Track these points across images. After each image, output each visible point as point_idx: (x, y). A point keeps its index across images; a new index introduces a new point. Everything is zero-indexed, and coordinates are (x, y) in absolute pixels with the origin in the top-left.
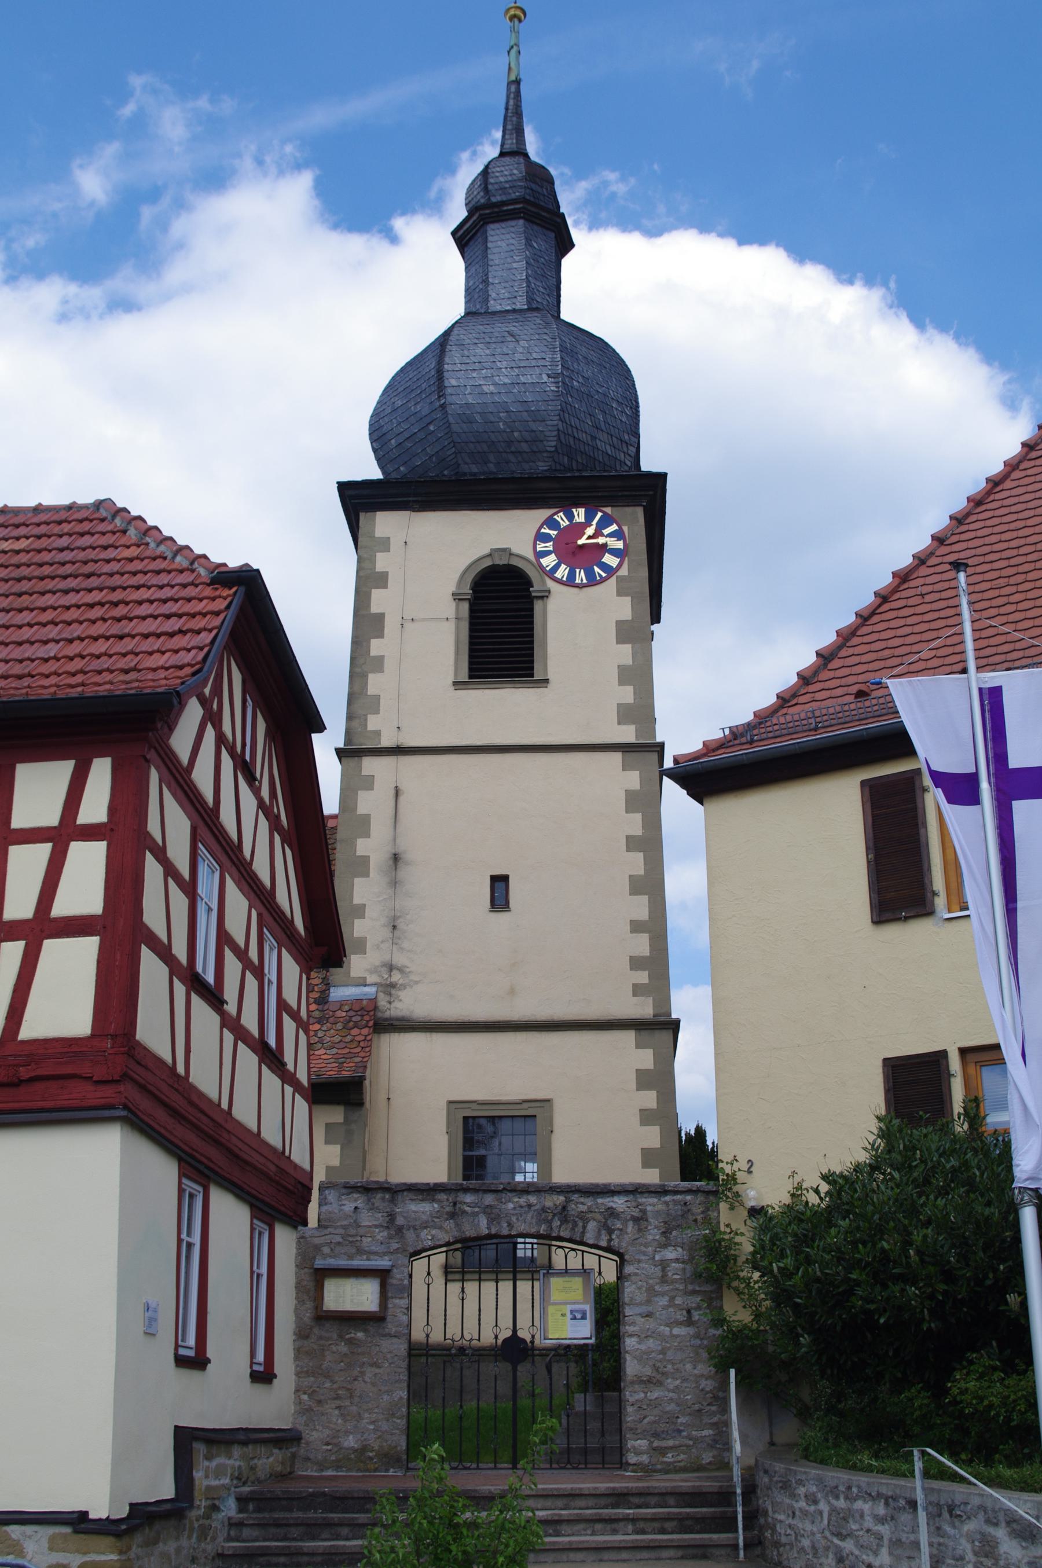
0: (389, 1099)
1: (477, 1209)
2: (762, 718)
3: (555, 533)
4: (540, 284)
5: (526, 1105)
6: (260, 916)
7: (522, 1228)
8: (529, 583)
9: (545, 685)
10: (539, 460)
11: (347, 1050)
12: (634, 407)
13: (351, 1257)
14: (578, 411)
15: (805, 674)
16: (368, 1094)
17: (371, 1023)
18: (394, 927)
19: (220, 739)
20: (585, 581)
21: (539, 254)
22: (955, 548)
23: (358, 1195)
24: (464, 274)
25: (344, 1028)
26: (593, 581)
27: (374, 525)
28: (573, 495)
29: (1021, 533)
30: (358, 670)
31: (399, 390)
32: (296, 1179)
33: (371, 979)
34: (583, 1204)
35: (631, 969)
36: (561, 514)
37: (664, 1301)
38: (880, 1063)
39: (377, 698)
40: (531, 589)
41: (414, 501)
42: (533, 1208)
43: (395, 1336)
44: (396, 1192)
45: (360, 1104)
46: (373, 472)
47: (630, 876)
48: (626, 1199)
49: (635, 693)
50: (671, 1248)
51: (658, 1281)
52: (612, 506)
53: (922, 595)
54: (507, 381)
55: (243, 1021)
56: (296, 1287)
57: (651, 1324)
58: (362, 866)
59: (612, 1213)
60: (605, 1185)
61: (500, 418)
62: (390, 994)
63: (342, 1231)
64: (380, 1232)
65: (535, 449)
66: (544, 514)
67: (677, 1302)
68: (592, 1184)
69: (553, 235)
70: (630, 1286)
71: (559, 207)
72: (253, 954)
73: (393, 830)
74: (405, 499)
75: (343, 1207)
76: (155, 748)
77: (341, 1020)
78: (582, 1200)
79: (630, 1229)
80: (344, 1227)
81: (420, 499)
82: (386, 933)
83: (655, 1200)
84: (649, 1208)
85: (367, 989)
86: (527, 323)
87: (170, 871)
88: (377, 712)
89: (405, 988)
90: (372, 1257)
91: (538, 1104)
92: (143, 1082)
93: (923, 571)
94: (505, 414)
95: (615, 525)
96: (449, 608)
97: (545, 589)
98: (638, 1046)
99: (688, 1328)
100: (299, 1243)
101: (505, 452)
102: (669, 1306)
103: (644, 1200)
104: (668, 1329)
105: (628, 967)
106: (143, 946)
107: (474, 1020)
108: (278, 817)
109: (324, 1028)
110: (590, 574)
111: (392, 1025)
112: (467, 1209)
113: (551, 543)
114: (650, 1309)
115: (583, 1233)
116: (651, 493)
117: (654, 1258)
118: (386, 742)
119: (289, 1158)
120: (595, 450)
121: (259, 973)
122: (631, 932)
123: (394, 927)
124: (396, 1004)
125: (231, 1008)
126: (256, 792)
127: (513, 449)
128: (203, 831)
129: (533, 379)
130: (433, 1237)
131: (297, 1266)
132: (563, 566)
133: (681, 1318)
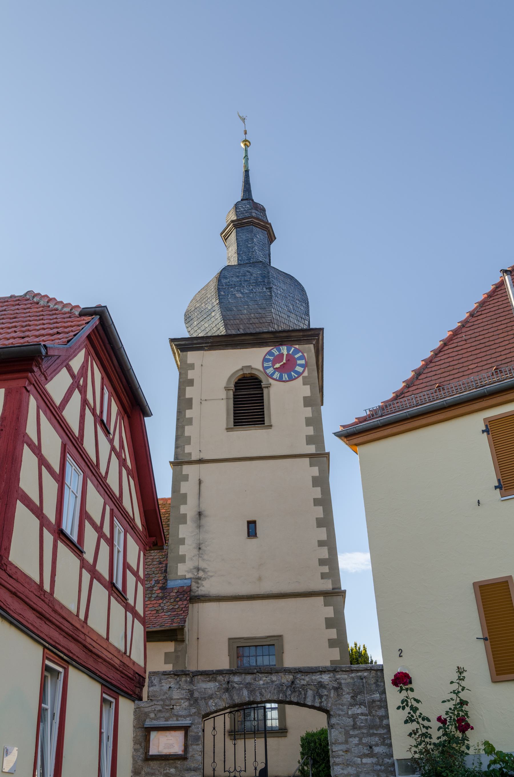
0: (198, 638)
1: (241, 686)
3: (272, 358)
4: (261, 253)
5: (269, 639)
6: (112, 510)
7: (268, 697)
8: (261, 382)
9: (270, 428)
10: (264, 327)
11: (176, 613)
12: (306, 303)
13: (167, 720)
14: (281, 304)
16: (187, 636)
17: (188, 598)
18: (200, 548)
19: (85, 402)
20: (287, 379)
21: (260, 240)
22: (479, 318)
23: (172, 680)
25: (174, 601)
26: (291, 379)
32: (134, 671)
33: (188, 576)
34: (304, 680)
36: (275, 349)
37: (356, 741)
39: (189, 438)
40: (262, 384)
41: (205, 346)
43: (193, 770)
45: (183, 641)
47: (317, 518)
48: (329, 676)
49: (314, 430)
50: (357, 706)
51: (351, 728)
53: (466, 340)
54: (247, 291)
55: (98, 568)
56: (133, 740)
57: (348, 756)
58: (183, 519)
59: (321, 685)
60: (316, 668)
62: (198, 583)
64: (184, 702)
65: (261, 321)
66: (267, 349)
67: (364, 742)
68: (308, 667)
70: (335, 731)
72: (106, 530)
73: (198, 500)
74: (201, 345)
75: (162, 688)
76: (34, 385)
77: (173, 597)
78: (303, 677)
79: (332, 695)
80: (162, 700)
81: (208, 345)
82: (196, 552)
83: (346, 676)
84: (343, 681)
85: (186, 581)
86: (256, 267)
87: (43, 462)
89: (206, 580)
92: (14, 590)
93: (464, 330)
94: (247, 306)
95: (300, 353)
96: (223, 394)
97: (268, 383)
99: (371, 758)
100: (135, 712)
102: (359, 744)
103: (339, 676)
104: (359, 759)
105: (318, 564)
106: (18, 501)
108: (125, 460)
109: (164, 602)
110: (290, 376)
112: (236, 685)
113: (271, 363)
115: (305, 698)
116: (317, 338)
117: (348, 713)
118: (194, 458)
119: (129, 657)
120: (290, 322)
121: (111, 542)
122: (319, 546)
123: (200, 548)
124: (201, 588)
125: (89, 557)
126: (111, 441)
127: (251, 322)
128: (69, 446)
129: (259, 290)
130: (216, 704)
131: (134, 726)
132: (277, 373)
133: (367, 752)
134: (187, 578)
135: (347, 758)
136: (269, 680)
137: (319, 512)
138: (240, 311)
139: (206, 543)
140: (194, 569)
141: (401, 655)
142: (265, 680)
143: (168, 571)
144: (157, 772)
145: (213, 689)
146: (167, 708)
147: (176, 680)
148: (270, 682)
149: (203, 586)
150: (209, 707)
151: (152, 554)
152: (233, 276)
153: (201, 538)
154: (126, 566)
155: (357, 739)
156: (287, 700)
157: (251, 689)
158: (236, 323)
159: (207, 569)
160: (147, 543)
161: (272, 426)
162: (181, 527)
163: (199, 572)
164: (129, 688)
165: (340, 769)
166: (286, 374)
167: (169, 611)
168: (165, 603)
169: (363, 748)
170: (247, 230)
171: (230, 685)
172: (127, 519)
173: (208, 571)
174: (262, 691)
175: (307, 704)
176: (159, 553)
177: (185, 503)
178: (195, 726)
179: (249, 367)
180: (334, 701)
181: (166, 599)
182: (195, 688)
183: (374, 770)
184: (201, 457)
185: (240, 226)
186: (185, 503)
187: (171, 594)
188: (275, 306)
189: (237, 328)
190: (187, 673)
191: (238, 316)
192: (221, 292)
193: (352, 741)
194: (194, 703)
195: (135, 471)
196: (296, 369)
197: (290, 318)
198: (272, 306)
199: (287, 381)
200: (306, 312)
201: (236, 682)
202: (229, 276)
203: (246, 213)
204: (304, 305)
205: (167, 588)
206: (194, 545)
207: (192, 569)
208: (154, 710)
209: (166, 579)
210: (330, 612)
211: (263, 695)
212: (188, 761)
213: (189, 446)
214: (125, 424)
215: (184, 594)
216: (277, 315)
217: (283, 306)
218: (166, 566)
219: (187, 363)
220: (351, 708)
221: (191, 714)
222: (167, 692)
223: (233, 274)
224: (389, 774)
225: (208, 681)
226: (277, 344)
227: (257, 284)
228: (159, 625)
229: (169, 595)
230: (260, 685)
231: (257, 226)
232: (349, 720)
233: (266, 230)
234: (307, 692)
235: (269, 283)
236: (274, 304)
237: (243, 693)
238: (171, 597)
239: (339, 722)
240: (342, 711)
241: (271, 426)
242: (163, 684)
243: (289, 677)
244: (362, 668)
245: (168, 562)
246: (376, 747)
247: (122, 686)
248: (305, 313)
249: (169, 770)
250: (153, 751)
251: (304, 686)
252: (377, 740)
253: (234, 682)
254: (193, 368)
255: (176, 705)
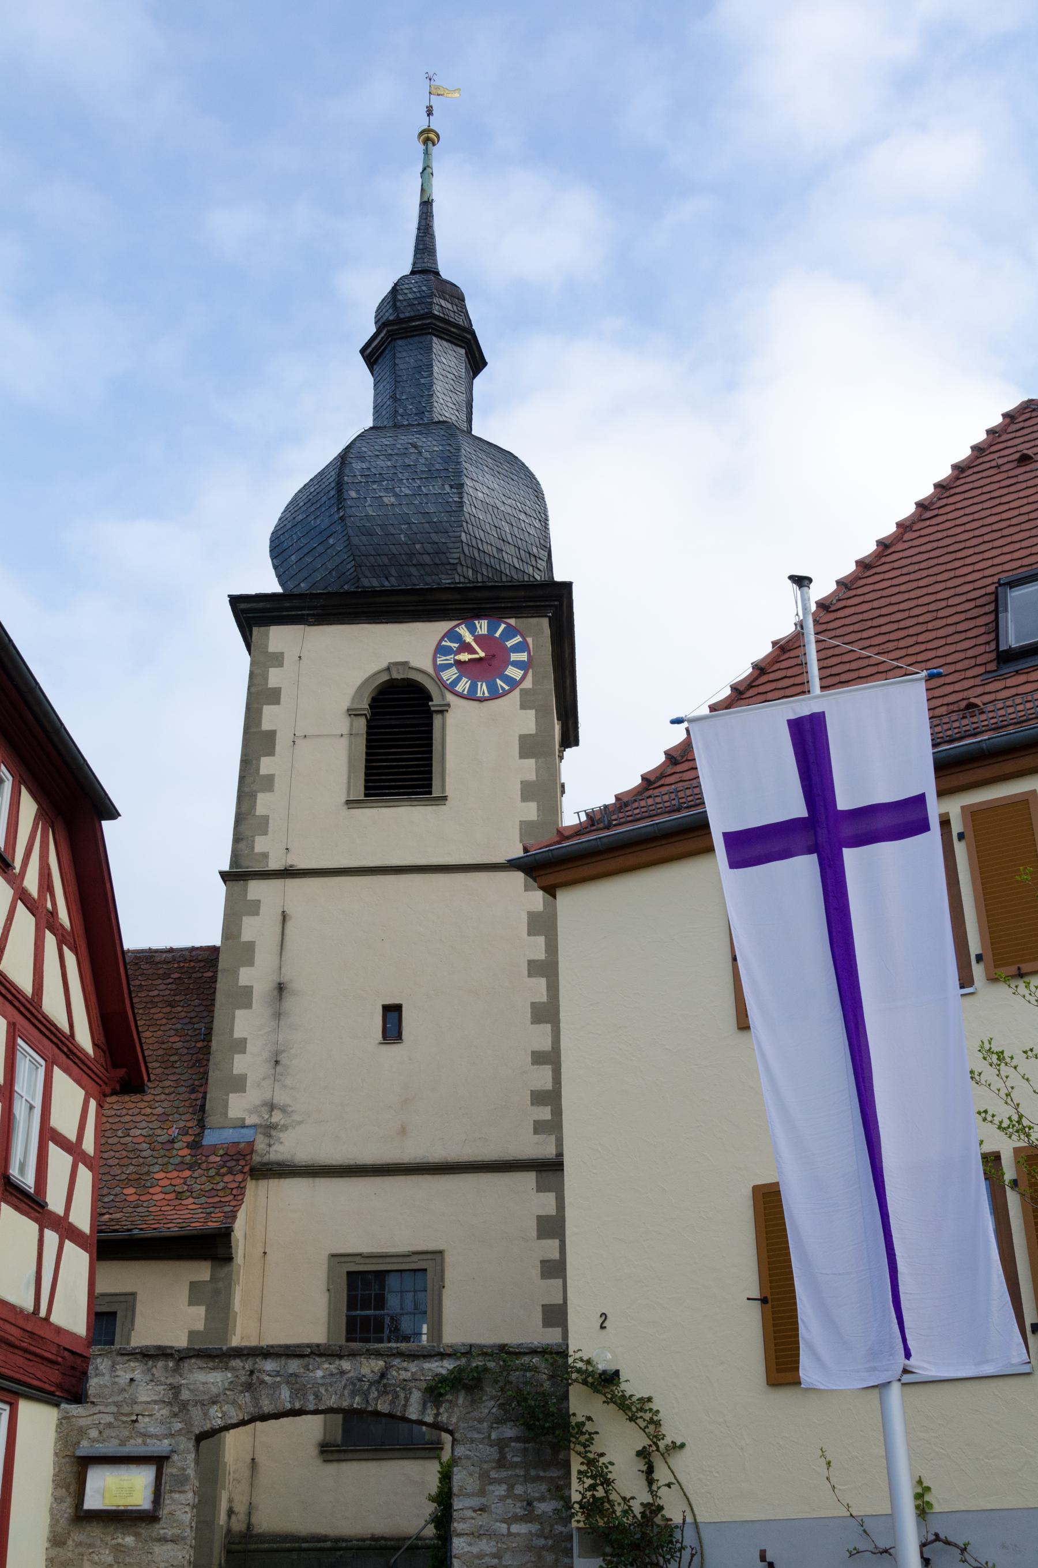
0: (265, 1253)
1: (278, 1379)
2: (623, 802)
3: (457, 645)
4: (449, 400)
5: (415, 1258)
10: (442, 574)
11: (217, 1199)
15: (673, 754)
17: (247, 1169)
20: (487, 694)
22: (841, 614)
23: (137, 1364)
24: (372, 392)
26: (495, 695)
27: (268, 639)
28: (475, 606)
29: (913, 594)
30: (247, 790)
31: (301, 505)
32: (59, 1346)
34: (406, 1370)
35: (532, 1104)
36: (463, 626)
38: (749, 1192)
39: (266, 819)
40: (430, 703)
41: (308, 615)
42: (345, 1377)
43: (171, 1541)
44: (181, 1359)
45: (229, 1259)
46: (272, 585)
47: (532, 1003)
49: (538, 810)
51: (494, 1465)
52: (515, 617)
54: (408, 492)
56: (54, 1481)
57: (483, 1520)
58: (244, 998)
61: (401, 530)
62: (270, 1136)
63: (114, 1409)
64: (160, 1409)
65: (437, 561)
66: (445, 626)
67: (516, 1492)
69: (463, 351)
70: (460, 1471)
71: (472, 325)
74: (300, 613)
75: (117, 1380)
77: (215, 1165)
78: (405, 1364)
80: (116, 1404)
81: (315, 612)
88: (265, 833)
90: (148, 1441)
91: (429, 1256)
94: (406, 526)
95: (519, 637)
96: (343, 725)
98: (539, 1189)
99: (529, 1525)
100: (60, 1425)
101: (407, 565)
102: (506, 1497)
104: (505, 1526)
107: (361, 1163)
108: (53, 914)
109: (196, 1175)
111: (271, 1170)
112: (267, 1378)
114: (484, 1500)
115: (405, 1406)
117: (489, 1437)
118: (274, 864)
119: (47, 1319)
120: (502, 563)
123: (277, 1062)
127: (415, 562)
129: (435, 489)
130: (224, 1414)
132: (464, 680)
133: (520, 1512)
134: (246, 1125)
135: (480, 1523)
136: (335, 1368)
137: (539, 988)
138: (391, 537)
139: (293, 1051)
140: (262, 1106)
141: (604, 1325)
142: (327, 1368)
143: (206, 1108)
144: (99, 1542)
145: (220, 1384)
146: (125, 1419)
147: (146, 1364)
148: (337, 1374)
149: (282, 1143)
150: (210, 1420)
151: (177, 1071)
152: (379, 454)
153: (281, 1040)
154: (48, 1135)
155: (504, 1487)
156: (370, 1409)
157: (297, 1386)
158: (381, 564)
159: (290, 1106)
160: (106, 1080)
161: (447, 800)
162: (239, 1013)
163: (273, 1113)
164: (47, 1381)
165: (464, 1544)
166: (484, 684)
167: (204, 1196)
168: (196, 1178)
169: (515, 1505)
170: (420, 345)
171: (254, 1377)
172: (52, 1037)
173: (292, 1111)
174: (319, 1391)
175: (410, 1417)
176: (191, 1067)
177: (250, 963)
178: (180, 1456)
179: (405, 664)
180: (464, 1412)
181: (200, 1168)
182: (183, 1382)
183: (532, 1547)
184: (290, 862)
185: (404, 335)
186: (250, 963)
187: (211, 1157)
188: (470, 527)
189: (384, 574)
190: (169, 1351)
191: (387, 547)
192: (349, 492)
193: (494, 1491)
194: (179, 1411)
195: (80, 932)
196: (506, 673)
197: (504, 553)
198: (462, 526)
199: (487, 699)
200: (542, 542)
201: (268, 1371)
202: (370, 453)
203: (419, 304)
204: (537, 524)
205: (202, 1146)
206: (266, 1055)
207: (258, 1106)
208: (97, 1422)
209: (202, 1125)
210: (546, 1204)
211: (321, 1399)
212: (161, 1522)
213: (264, 837)
214: (57, 836)
215: (239, 1160)
216: (473, 547)
217: (488, 526)
218: (204, 1098)
219: (267, 652)
220: (498, 1428)
221: (173, 1432)
222: (126, 1388)
223: (379, 451)
224: (561, 1554)
225: (212, 1369)
226: (469, 615)
227: (431, 475)
228: (178, 1225)
229: (206, 1161)
230: (316, 1378)
231: (442, 335)
232: (492, 1449)
233: (463, 345)
234: (411, 1393)
235: (459, 473)
236: (467, 523)
237: (280, 1394)
238: (211, 1165)
239: (470, 1453)
240: (478, 1433)
241: (444, 798)
242: (119, 1373)
243: (376, 1365)
244: (525, 1348)
245: (209, 1090)
246: (539, 1502)
247: (29, 1377)
248: (538, 545)
249: (123, 1539)
250: (91, 1502)
251: (405, 1383)
252: (543, 1490)
253: (264, 1371)
254: (281, 665)
255: (143, 1415)
